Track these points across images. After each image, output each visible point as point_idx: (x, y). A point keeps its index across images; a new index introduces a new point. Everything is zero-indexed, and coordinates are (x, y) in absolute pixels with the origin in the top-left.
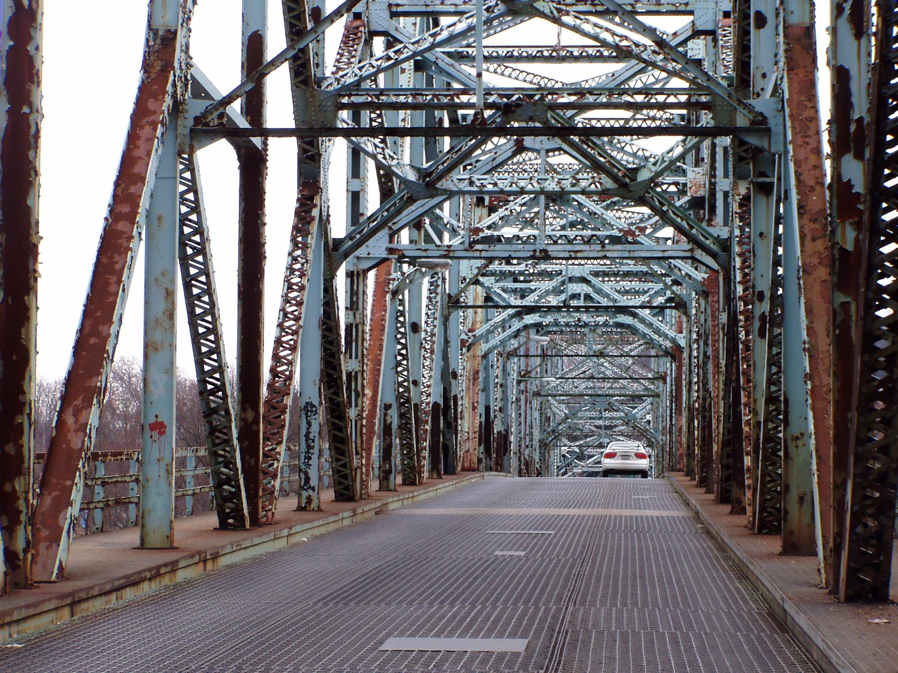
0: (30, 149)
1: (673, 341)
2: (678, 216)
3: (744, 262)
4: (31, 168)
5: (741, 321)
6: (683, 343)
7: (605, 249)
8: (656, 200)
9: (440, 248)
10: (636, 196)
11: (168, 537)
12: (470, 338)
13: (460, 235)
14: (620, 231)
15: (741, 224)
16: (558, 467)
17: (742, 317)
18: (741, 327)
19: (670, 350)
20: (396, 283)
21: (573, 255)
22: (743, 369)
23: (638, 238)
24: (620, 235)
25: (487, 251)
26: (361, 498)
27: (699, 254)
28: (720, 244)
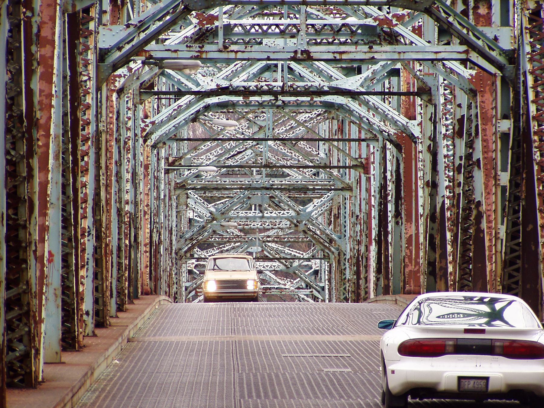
0: (32, 44)
1: (405, 129)
2: (464, 27)
3: (536, 80)
4: (34, 59)
5: (535, 141)
6: (416, 132)
7: (373, 50)
8: (442, 11)
9: (191, 49)
10: (422, 7)
11: (57, 353)
12: (147, 126)
13: (191, 23)
14: (375, 19)
15: (532, 40)
16: (186, 289)
17: (536, 138)
18: (536, 147)
19: (394, 138)
20: (122, 80)
21: (338, 56)
22: (539, 190)
23: (396, 28)
24: (375, 24)
25: (243, 52)
26: (110, 325)
27: (474, 56)
28: (507, 56)
